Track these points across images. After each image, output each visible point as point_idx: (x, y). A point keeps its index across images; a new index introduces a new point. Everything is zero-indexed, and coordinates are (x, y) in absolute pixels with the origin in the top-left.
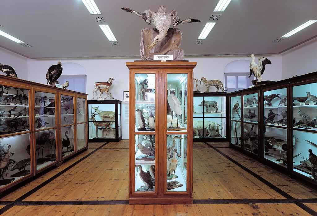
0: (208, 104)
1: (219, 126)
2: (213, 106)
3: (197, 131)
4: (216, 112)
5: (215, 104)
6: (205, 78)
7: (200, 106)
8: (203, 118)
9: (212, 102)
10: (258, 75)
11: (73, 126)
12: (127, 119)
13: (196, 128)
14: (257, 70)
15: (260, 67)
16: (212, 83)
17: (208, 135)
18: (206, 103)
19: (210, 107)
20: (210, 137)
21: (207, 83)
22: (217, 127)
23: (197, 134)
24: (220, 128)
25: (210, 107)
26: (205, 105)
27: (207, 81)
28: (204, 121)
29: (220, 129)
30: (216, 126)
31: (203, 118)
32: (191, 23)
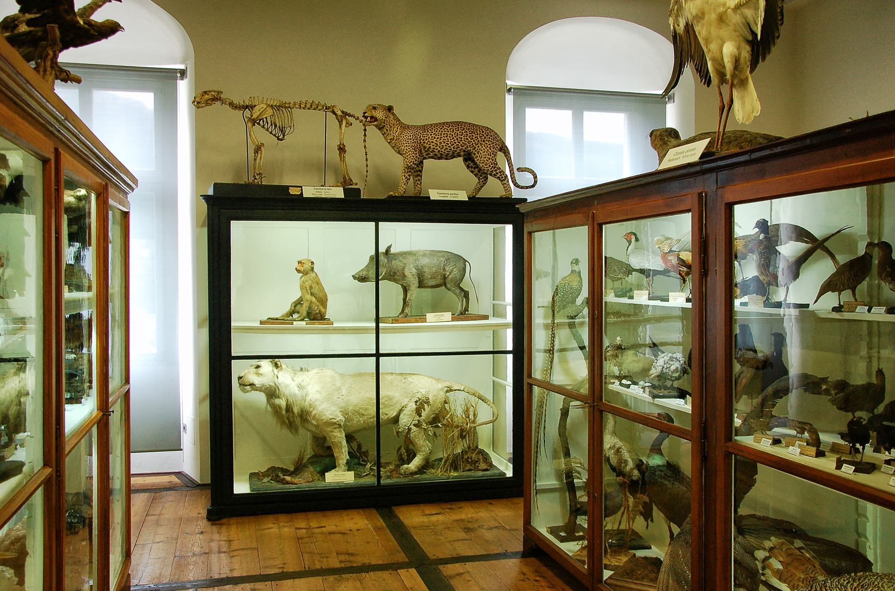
0: (410, 272)
1: (473, 399)
2: (438, 281)
3: (339, 437)
4: (464, 314)
5: (452, 271)
6: (390, 109)
7: (362, 279)
8: (378, 355)
9: (434, 253)
10: (729, 66)
11: (872, 415)
12: (847, 448)
13: (340, 418)
14: (724, 32)
15: (748, 12)
16: (434, 141)
17: (411, 456)
18: (397, 264)
19: (421, 285)
20: (422, 469)
21: (407, 141)
22: (467, 411)
23: (343, 455)
24: (484, 413)
25: (421, 285)
26: (392, 276)
27: (405, 127)
28: (373, 336)
29: (481, 419)
30: (457, 409)
31: (378, 355)
32: (399, 446)
